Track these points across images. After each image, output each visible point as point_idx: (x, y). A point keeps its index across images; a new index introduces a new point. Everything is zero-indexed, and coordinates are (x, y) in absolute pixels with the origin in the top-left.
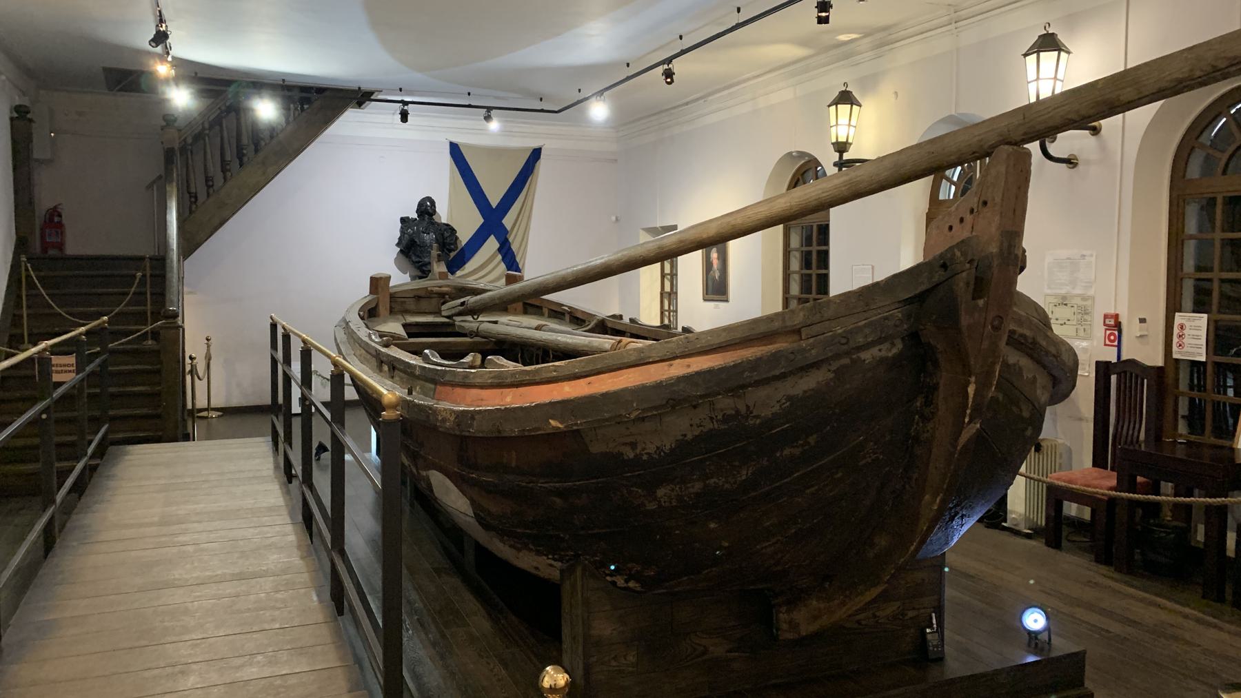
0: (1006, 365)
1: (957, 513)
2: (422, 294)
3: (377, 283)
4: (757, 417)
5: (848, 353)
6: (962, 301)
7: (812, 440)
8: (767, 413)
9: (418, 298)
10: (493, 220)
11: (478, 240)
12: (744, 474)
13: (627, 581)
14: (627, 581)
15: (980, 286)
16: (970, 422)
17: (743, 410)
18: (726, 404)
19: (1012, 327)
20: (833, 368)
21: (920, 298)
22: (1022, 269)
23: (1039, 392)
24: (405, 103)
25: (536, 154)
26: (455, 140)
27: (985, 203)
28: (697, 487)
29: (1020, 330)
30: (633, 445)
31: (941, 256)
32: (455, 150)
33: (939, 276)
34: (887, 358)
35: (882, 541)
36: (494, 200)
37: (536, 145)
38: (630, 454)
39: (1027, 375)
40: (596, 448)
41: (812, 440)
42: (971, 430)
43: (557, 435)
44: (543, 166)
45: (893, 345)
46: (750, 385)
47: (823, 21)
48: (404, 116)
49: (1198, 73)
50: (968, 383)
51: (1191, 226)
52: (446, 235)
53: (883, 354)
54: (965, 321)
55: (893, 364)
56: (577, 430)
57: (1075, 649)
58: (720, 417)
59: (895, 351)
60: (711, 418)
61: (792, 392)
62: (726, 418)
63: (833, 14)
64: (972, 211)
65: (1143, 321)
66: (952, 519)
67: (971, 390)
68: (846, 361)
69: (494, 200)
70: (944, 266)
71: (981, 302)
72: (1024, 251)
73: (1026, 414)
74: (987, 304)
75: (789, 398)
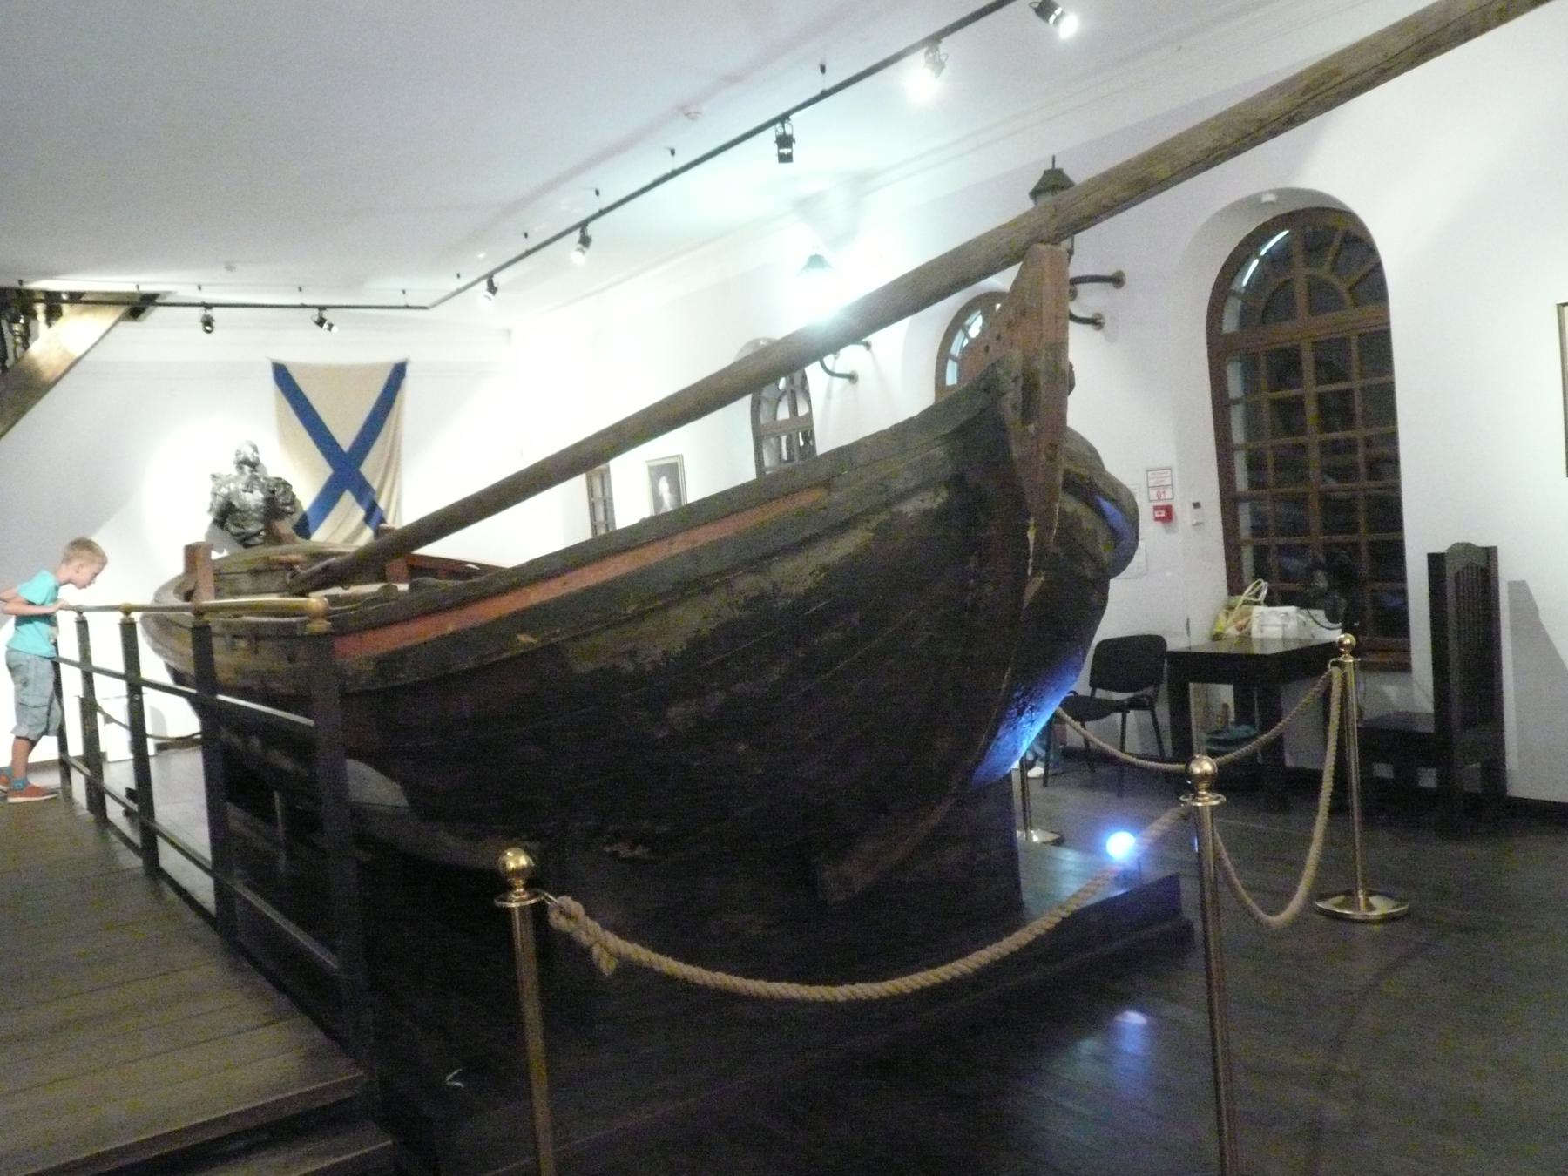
0: (1063, 512)
1: (1025, 705)
2: (260, 566)
3: (193, 554)
4: (787, 596)
5: (886, 505)
6: (999, 466)
7: (855, 618)
8: (798, 589)
9: (256, 572)
10: (347, 473)
11: (328, 499)
12: (775, 674)
13: (632, 849)
14: (632, 849)
15: (1028, 407)
16: (1033, 575)
17: (768, 587)
18: (747, 583)
19: (1067, 465)
20: (874, 524)
21: (961, 431)
22: (1072, 387)
23: (1101, 548)
24: (208, 306)
25: (399, 371)
26: (284, 357)
27: (1024, 314)
28: (718, 698)
29: (1074, 469)
30: (632, 654)
31: (983, 378)
32: (283, 376)
33: (980, 402)
34: (931, 510)
35: (944, 744)
36: (345, 438)
37: (397, 358)
38: (628, 666)
39: (1086, 525)
40: (583, 666)
41: (855, 618)
42: (1035, 584)
43: (530, 655)
44: (409, 385)
45: (937, 495)
46: (777, 553)
47: (786, 159)
48: (208, 322)
49: (1229, 141)
50: (1027, 527)
51: (1235, 388)
52: (277, 503)
53: (927, 505)
54: (1016, 451)
55: (941, 516)
56: (553, 645)
57: (1169, 873)
58: (741, 601)
59: (939, 500)
60: (730, 605)
61: (827, 559)
62: (751, 603)
63: (797, 150)
64: (1009, 325)
65: (1197, 505)
66: (1020, 714)
67: (1031, 535)
68: (885, 516)
69: (345, 438)
70: (987, 390)
71: (1031, 428)
72: (1071, 366)
73: (1089, 574)
74: (1039, 431)
75: (825, 568)
